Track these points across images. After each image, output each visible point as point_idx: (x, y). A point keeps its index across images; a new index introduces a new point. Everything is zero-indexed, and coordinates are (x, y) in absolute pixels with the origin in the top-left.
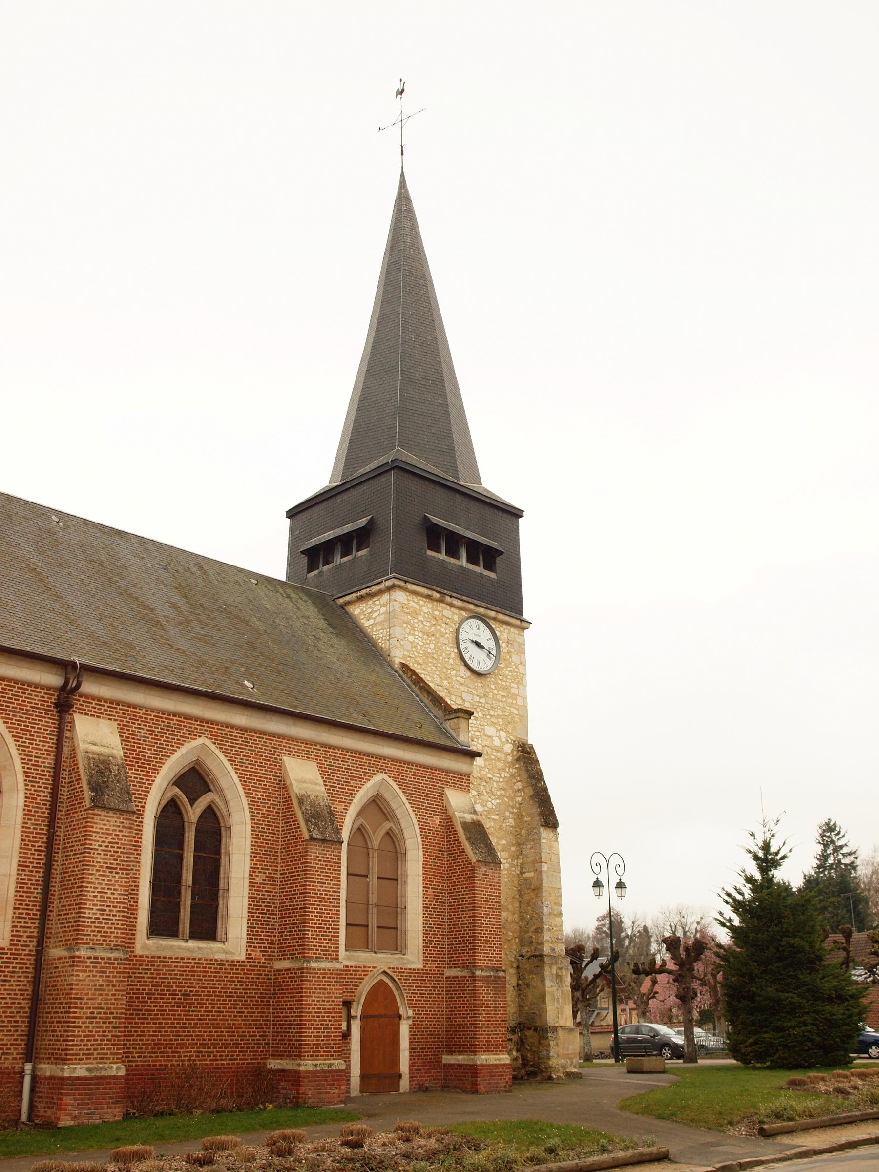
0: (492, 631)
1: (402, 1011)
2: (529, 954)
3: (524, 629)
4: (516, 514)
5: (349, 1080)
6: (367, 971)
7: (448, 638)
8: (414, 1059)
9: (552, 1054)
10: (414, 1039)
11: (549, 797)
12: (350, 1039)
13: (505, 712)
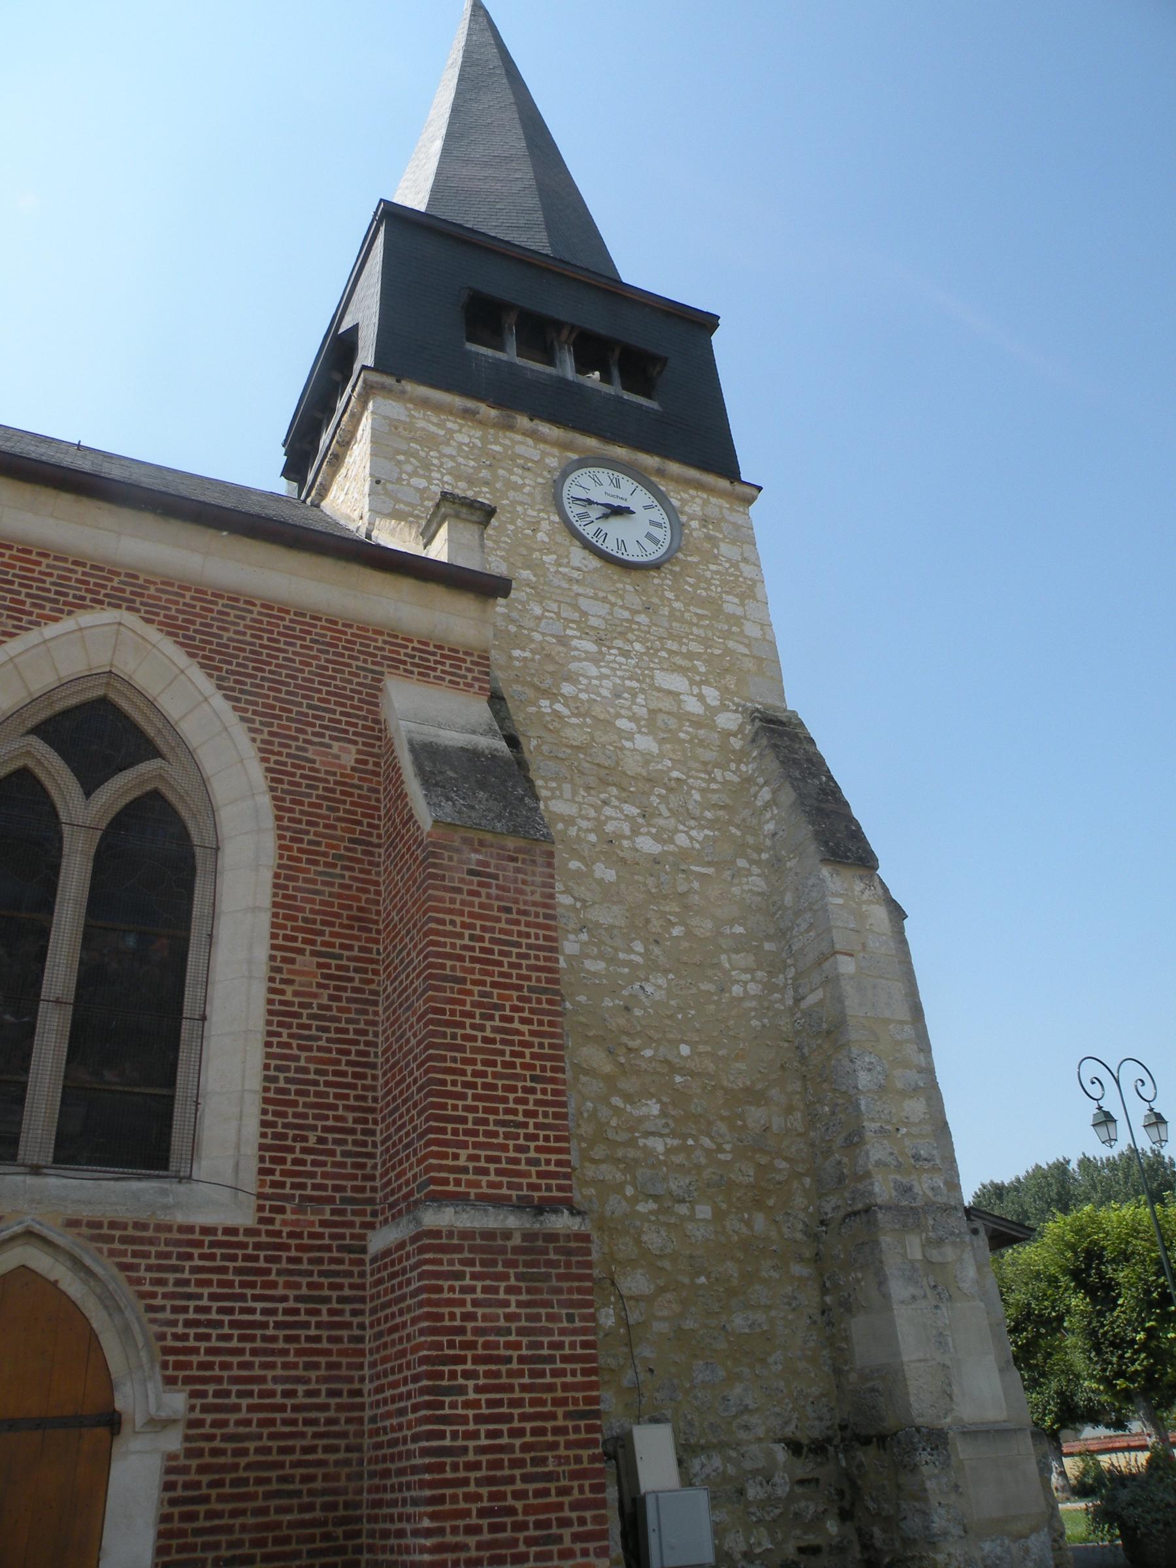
0: (662, 499)
2: (842, 1213)
3: (750, 501)
4: (707, 323)
7: (530, 494)
9: (938, 1524)
10: (190, 1517)
11: (846, 804)
13: (710, 647)
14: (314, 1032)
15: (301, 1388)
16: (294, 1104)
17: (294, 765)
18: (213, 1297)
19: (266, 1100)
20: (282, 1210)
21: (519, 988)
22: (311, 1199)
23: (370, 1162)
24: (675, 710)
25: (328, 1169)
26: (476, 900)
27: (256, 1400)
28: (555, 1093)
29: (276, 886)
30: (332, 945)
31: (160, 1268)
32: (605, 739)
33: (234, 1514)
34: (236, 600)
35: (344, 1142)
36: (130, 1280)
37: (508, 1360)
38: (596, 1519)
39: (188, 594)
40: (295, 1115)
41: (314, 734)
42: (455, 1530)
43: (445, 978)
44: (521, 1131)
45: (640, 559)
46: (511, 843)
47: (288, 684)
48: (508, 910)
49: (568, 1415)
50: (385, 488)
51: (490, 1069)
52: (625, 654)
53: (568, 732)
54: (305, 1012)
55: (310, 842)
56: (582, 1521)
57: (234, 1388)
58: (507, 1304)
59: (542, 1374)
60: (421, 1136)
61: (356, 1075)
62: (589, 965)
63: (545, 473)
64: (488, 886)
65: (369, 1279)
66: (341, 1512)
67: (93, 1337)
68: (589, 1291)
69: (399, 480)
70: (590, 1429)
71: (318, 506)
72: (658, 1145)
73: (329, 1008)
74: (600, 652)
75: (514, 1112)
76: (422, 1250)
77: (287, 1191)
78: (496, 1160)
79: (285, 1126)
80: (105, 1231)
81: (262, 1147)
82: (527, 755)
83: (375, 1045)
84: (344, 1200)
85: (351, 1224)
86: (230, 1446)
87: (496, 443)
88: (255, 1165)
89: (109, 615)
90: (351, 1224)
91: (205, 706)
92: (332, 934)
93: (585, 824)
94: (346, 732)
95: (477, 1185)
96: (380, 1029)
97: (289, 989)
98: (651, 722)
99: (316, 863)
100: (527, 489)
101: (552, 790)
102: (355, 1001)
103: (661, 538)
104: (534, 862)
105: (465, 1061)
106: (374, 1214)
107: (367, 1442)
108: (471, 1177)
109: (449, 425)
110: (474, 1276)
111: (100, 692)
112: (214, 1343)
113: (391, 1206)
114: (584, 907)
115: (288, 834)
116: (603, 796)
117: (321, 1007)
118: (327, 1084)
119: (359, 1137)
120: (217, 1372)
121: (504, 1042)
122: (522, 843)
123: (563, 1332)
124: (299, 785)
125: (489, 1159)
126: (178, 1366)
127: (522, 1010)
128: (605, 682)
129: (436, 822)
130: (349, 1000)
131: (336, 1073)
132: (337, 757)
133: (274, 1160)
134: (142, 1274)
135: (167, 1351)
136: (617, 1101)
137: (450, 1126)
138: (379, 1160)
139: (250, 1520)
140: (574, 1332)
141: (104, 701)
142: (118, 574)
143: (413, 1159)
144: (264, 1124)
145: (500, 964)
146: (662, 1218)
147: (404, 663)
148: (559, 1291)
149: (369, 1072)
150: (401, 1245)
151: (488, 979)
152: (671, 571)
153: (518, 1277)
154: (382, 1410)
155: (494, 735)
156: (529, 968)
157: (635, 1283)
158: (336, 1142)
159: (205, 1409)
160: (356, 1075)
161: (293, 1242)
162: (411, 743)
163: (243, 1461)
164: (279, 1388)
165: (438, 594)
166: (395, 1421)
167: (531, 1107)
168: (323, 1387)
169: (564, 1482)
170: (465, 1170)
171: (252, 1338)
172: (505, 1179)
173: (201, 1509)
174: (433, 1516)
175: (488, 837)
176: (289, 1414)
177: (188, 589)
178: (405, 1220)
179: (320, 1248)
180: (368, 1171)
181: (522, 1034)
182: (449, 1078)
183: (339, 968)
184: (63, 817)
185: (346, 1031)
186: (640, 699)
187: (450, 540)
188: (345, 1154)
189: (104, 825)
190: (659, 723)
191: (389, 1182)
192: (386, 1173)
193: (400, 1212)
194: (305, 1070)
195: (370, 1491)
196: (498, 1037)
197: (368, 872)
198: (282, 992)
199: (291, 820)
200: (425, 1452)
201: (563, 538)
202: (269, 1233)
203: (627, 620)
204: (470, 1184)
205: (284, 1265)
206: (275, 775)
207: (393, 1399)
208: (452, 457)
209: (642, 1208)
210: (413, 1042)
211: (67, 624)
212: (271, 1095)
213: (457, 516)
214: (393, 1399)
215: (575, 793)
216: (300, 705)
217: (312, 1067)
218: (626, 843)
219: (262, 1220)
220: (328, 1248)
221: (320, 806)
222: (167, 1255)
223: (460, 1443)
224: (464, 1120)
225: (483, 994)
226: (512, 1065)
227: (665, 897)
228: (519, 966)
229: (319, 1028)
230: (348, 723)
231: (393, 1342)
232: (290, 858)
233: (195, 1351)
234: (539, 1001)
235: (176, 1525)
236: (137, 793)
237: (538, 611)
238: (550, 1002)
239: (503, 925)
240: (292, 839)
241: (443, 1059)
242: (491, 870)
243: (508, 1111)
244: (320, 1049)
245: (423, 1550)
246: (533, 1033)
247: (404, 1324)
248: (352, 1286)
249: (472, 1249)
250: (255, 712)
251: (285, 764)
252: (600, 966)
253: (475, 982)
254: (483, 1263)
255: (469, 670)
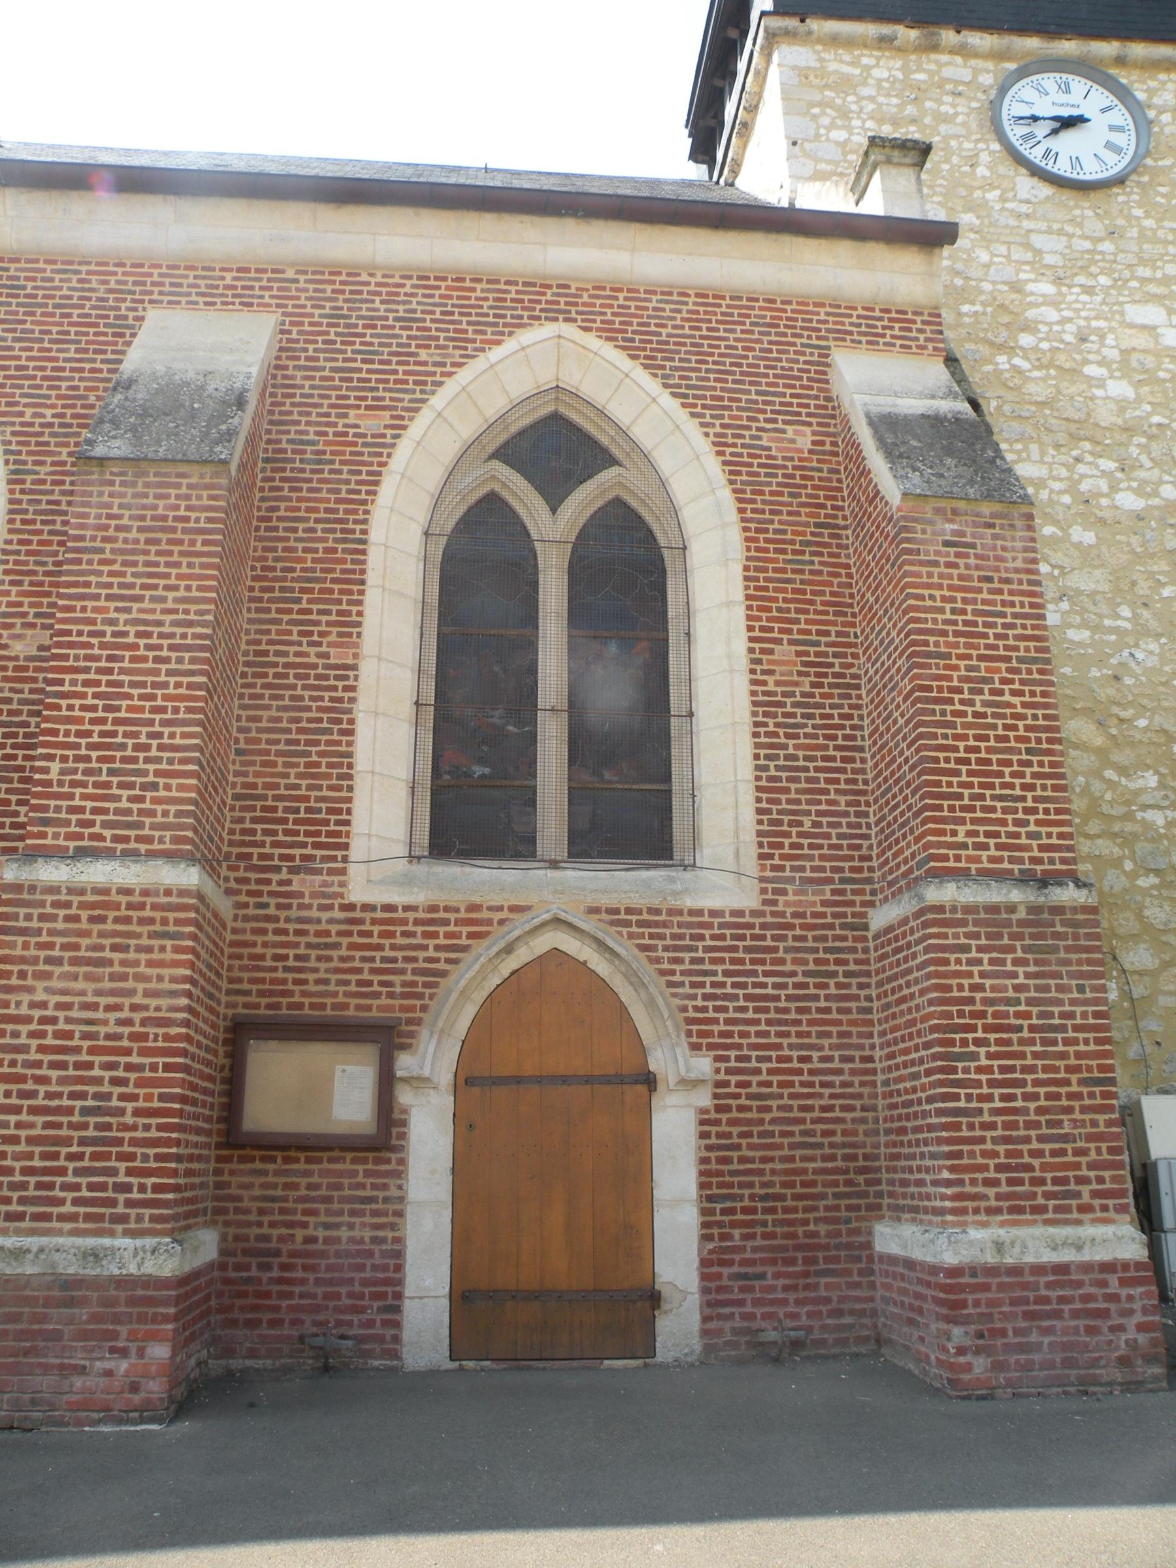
0: (1123, 94)
1: (657, 1062)
5: (397, 1309)
6: (489, 922)
7: (964, 124)
8: (724, 1237)
12: (402, 1162)
14: (799, 720)
15: (815, 1055)
16: (787, 790)
17: (750, 455)
18: (726, 973)
19: (759, 789)
20: (784, 892)
21: (1008, 659)
22: (811, 881)
23: (865, 843)
24: (1151, 346)
25: (825, 851)
26: (955, 572)
27: (775, 1065)
28: (1052, 764)
29: (746, 579)
30: (809, 632)
31: (676, 948)
32: (1073, 390)
33: (764, 1160)
34: (670, 293)
35: (839, 825)
36: (650, 959)
37: (1019, 1029)
38: (1114, 1179)
39: (621, 296)
40: (789, 802)
41: (766, 420)
42: (973, 1182)
43: (929, 655)
44: (1020, 805)
45: (1100, 176)
46: (986, 509)
47: (733, 373)
48: (989, 579)
49: (1081, 1082)
50: (803, 150)
51: (982, 745)
52: (1089, 290)
53: (1031, 388)
54: (788, 701)
55: (776, 531)
56: (1100, 1180)
57: (754, 1054)
58: (1014, 975)
59: (1054, 1042)
60: (917, 815)
61: (844, 760)
62: (1072, 634)
63: (980, 95)
64: (967, 556)
65: (873, 955)
66: (861, 1163)
67: (623, 1009)
68: (1100, 963)
69: (817, 136)
70: (1106, 1095)
71: (732, 185)
72: (1158, 818)
73: (812, 695)
74: (1060, 293)
75: (1011, 786)
76: (926, 925)
77: (788, 874)
78: (997, 835)
79: (779, 812)
80: (623, 916)
81: (760, 834)
82: (988, 418)
83: (861, 728)
84: (843, 881)
85: (852, 903)
86: (754, 1103)
87: (920, 69)
88: (754, 851)
89: (548, 330)
90: (852, 903)
91: (654, 407)
92: (807, 622)
93: (1057, 486)
94: (799, 414)
95: (978, 860)
96: (865, 712)
97: (770, 679)
98: (1124, 365)
99: (784, 551)
100: (960, 119)
101: (1018, 452)
102: (837, 686)
103: (1123, 145)
104: (1012, 526)
105: (956, 737)
106: (873, 893)
107: (881, 1103)
108: (971, 852)
109: (865, 61)
110: (980, 949)
111: (550, 408)
112: (731, 1014)
113: (891, 884)
114: (1063, 574)
115: (753, 526)
116: (1075, 453)
117: (803, 694)
118: (817, 769)
119: (853, 819)
120: (737, 1040)
121: (995, 715)
122: (997, 507)
123: (1073, 1002)
124: (758, 474)
125: (988, 834)
126: (701, 1034)
127: (1012, 681)
128: (1068, 327)
129: (905, 494)
130: (830, 686)
131: (825, 759)
132: (792, 441)
133: (772, 845)
134: (660, 953)
135: (690, 1021)
136: (1110, 774)
137: (946, 803)
138: (874, 841)
139: (778, 1166)
140: (1085, 1002)
141: (555, 417)
142: (549, 287)
143: (910, 838)
144: (760, 811)
145: (985, 636)
146: (1165, 892)
147: (851, 333)
148: (1068, 962)
149: (857, 755)
150: (904, 921)
151: (974, 653)
152: (1138, 183)
153: (1025, 949)
154: (895, 1074)
155: (956, 398)
156: (1016, 638)
157: (1138, 957)
158: (830, 825)
159: (729, 1071)
160: (844, 760)
161: (797, 921)
162: (868, 415)
163: (768, 1117)
164: (795, 1054)
165: (878, 252)
166: (908, 1085)
167: (1028, 780)
168: (836, 1054)
169: (1081, 1144)
170: (964, 846)
171: (766, 1010)
172: (1006, 854)
173: (735, 1154)
174: (952, 1169)
175: (962, 505)
176: (806, 1077)
177: (620, 290)
178: (906, 897)
179: (823, 927)
180: (864, 852)
181: (1014, 706)
182: (941, 755)
183: (817, 654)
184: (534, 535)
185: (831, 717)
186: (1110, 340)
187: (884, 190)
188: (840, 836)
189: (573, 538)
190: (1134, 364)
191: (886, 862)
192: (883, 852)
193: (900, 890)
194: (795, 758)
195: (887, 1146)
196: (989, 711)
197: (838, 556)
198: (764, 683)
199: (754, 511)
200: (940, 1112)
201: (1007, 168)
202: (773, 914)
203: (1088, 251)
204: (970, 859)
205: (790, 943)
206: (733, 467)
207: (905, 1065)
208: (871, 99)
209: (1142, 882)
210: (901, 721)
211: (510, 345)
212: (764, 783)
213: (889, 161)
214: (905, 1065)
215: (1043, 453)
216: (748, 392)
217: (801, 754)
218: (1104, 502)
219: (765, 902)
220: (831, 927)
221: (781, 494)
222: (681, 937)
223: (974, 1105)
224: (960, 797)
225: (969, 668)
226: (1006, 739)
227: (1152, 556)
228: (1006, 637)
229: (803, 716)
230: (799, 405)
231: (902, 1013)
232: (757, 549)
233: (715, 1021)
234: (1029, 672)
235: (714, 1166)
236: (600, 503)
237: (984, 257)
238: (1040, 672)
239: (985, 595)
240: (757, 530)
241: (934, 736)
242: (968, 539)
243: (1004, 786)
244: (806, 736)
245: (944, 1197)
246: (1024, 705)
247: (912, 996)
248: (856, 962)
249: (976, 923)
250: (704, 407)
251: (741, 455)
252: (1084, 635)
253: (960, 657)
254: (989, 936)
255: (920, 331)
